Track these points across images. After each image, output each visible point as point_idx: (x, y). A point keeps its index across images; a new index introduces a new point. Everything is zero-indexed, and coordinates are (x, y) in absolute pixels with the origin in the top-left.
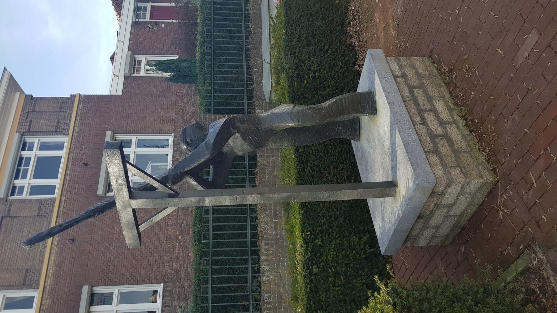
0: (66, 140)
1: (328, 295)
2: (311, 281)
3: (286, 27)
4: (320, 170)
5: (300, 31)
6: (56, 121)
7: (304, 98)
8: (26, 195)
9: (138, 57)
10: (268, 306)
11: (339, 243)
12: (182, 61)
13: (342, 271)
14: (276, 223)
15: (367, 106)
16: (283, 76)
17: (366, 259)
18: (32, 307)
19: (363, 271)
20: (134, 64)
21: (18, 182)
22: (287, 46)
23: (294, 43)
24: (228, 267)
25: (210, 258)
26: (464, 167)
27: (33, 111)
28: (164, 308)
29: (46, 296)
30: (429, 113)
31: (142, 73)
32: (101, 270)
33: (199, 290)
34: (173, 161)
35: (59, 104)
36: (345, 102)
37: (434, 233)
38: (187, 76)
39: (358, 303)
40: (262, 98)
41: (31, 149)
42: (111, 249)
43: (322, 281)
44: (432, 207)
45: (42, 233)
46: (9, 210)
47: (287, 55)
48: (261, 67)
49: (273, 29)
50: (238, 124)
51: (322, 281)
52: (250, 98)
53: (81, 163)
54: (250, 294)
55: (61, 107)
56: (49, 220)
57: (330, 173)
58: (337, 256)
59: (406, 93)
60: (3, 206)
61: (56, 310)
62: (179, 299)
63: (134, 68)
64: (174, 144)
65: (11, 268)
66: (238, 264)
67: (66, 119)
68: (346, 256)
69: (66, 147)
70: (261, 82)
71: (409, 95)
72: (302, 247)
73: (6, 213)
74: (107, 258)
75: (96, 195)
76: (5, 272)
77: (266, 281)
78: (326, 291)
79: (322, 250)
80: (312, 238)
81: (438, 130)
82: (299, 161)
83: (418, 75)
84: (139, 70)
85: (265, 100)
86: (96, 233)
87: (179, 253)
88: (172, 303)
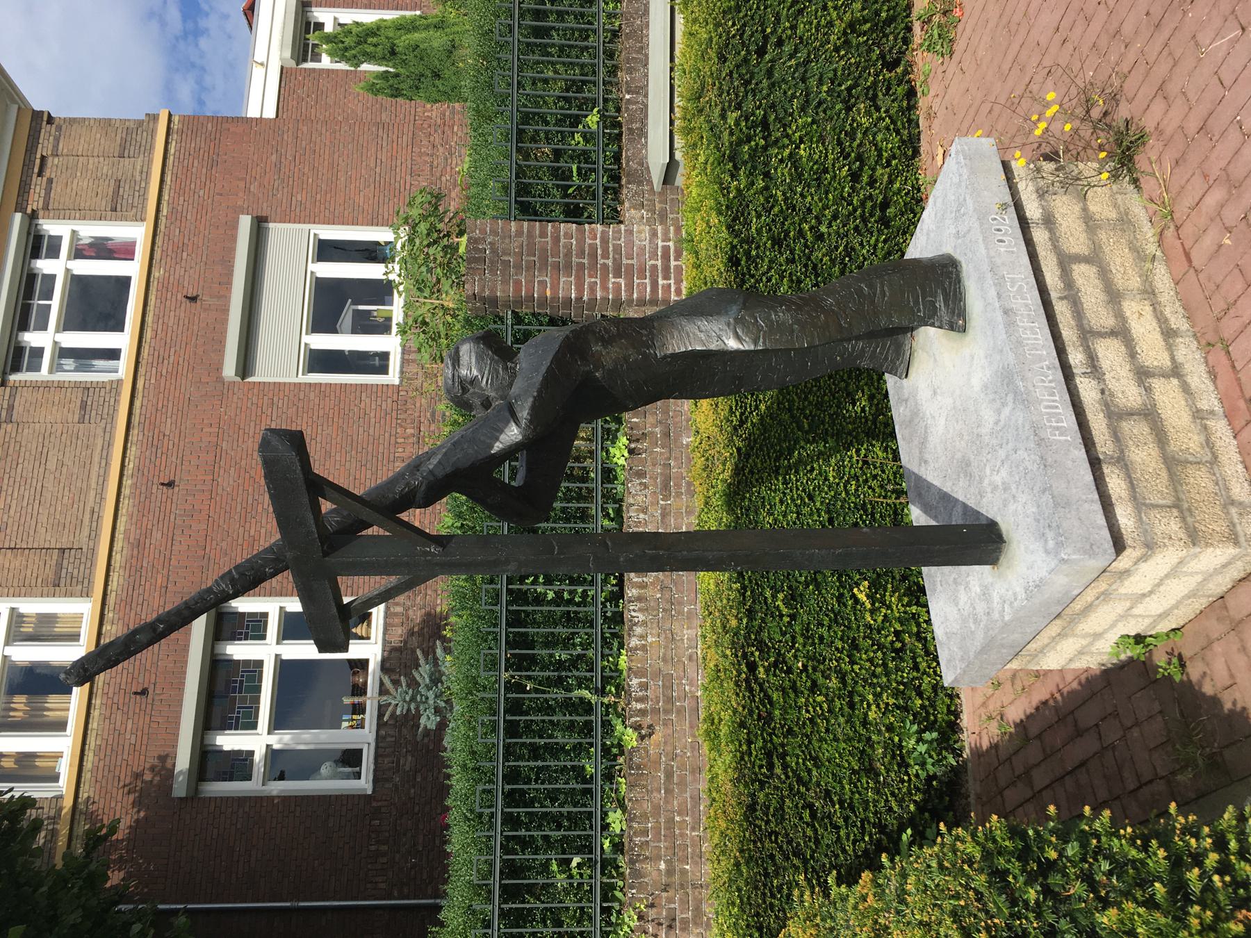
0: (136, 232)
6: (112, 182)
10: (639, 706)
14: (664, 508)
15: (940, 303)
21: (32, 338)
29: (111, 615)
35: (118, 138)
37: (1084, 647)
40: (641, 177)
41: (54, 253)
42: (260, 509)
46: (11, 408)
53: (179, 296)
55: (123, 147)
67: (138, 178)
70: (643, 133)
74: (252, 533)
75: (220, 379)
77: (636, 649)
85: (650, 182)
86: (222, 471)
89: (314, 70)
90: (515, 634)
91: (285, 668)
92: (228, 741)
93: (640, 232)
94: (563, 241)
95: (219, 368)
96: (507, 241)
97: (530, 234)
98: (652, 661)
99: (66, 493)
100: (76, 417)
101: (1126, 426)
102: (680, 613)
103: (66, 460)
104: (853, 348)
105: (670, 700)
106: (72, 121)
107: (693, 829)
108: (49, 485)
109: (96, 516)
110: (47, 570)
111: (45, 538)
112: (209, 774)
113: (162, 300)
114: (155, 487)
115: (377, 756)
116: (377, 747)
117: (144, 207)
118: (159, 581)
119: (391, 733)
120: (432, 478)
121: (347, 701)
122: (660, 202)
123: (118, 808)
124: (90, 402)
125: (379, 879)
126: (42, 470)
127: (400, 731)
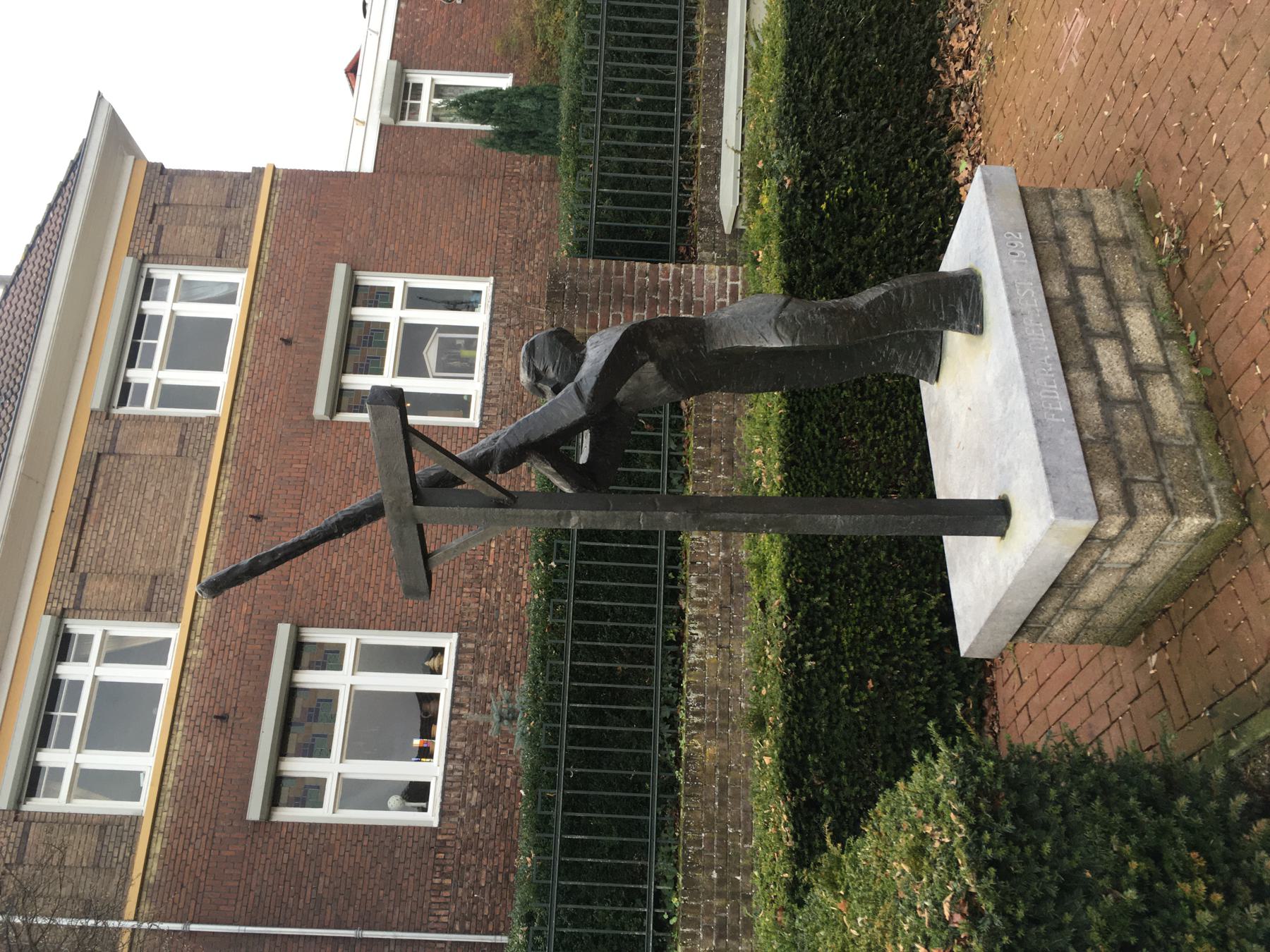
0: (241, 279)
1: (835, 720)
2: (798, 688)
3: (787, 64)
4: (839, 430)
5: (820, 74)
6: (219, 230)
7: (817, 249)
8: (152, 407)
9: (416, 76)
10: (696, 720)
11: (871, 608)
12: (522, 96)
13: (872, 670)
15: (961, 310)
16: (770, 184)
17: (929, 648)
18: (165, 663)
19: (921, 675)
20: (404, 95)
21: (136, 375)
22: (786, 113)
23: (803, 107)
24: (609, 624)
25: (570, 602)
26: (1172, 485)
27: (167, 204)
28: (457, 689)
30: (1108, 341)
31: (423, 119)
32: (320, 591)
33: (543, 669)
34: (489, 346)
35: (226, 189)
36: (909, 298)
38: (532, 134)
39: (901, 746)
40: (714, 220)
43: (824, 691)
44: (1085, 567)
45: (237, 567)
46: (114, 439)
47: (782, 137)
48: (715, 140)
49: (752, 61)
50: (654, 340)
51: (824, 691)
52: (683, 219)
53: (276, 338)
54: (657, 689)
55: (230, 197)
56: (203, 468)
57: (863, 440)
58: (863, 638)
59: (1059, 287)
60: (100, 429)
61: (217, 673)
62: (491, 672)
63: (404, 105)
64: (493, 305)
65: (120, 572)
66: (635, 620)
67: (243, 226)
68: (882, 638)
69: (242, 295)
71: (1066, 293)
72: (782, 609)
73: (108, 445)
74: (334, 566)
75: (311, 419)
76: (106, 578)
77: (695, 664)
78: (831, 713)
79: (829, 622)
80: (809, 591)
81: (1122, 383)
82: (792, 409)
83: (1098, 241)
84: (415, 110)
85: (721, 226)
87: (496, 567)
88: (476, 680)
89: (411, 128)
90: (574, 730)
91: (361, 698)
92: (297, 767)
93: (710, 271)
94: (637, 278)
95: (310, 407)
96: (585, 277)
97: (607, 272)
98: (711, 678)
99: (162, 521)
100: (175, 450)
101: (1118, 414)
102: (738, 632)
103: (163, 491)
104: (887, 355)
105: (725, 715)
106: (184, 173)
107: (745, 841)
108: (146, 514)
109: (188, 545)
110: (140, 595)
111: (139, 562)
112: (291, 747)
113: (260, 342)
114: (244, 519)
115: (445, 790)
116: (444, 781)
117: (247, 254)
118: (245, 609)
119: (459, 767)
120: (506, 447)
121: (417, 742)
122: (730, 244)
123: (195, 828)
124: (189, 437)
125: (442, 912)
126: (140, 499)
127: (467, 766)
